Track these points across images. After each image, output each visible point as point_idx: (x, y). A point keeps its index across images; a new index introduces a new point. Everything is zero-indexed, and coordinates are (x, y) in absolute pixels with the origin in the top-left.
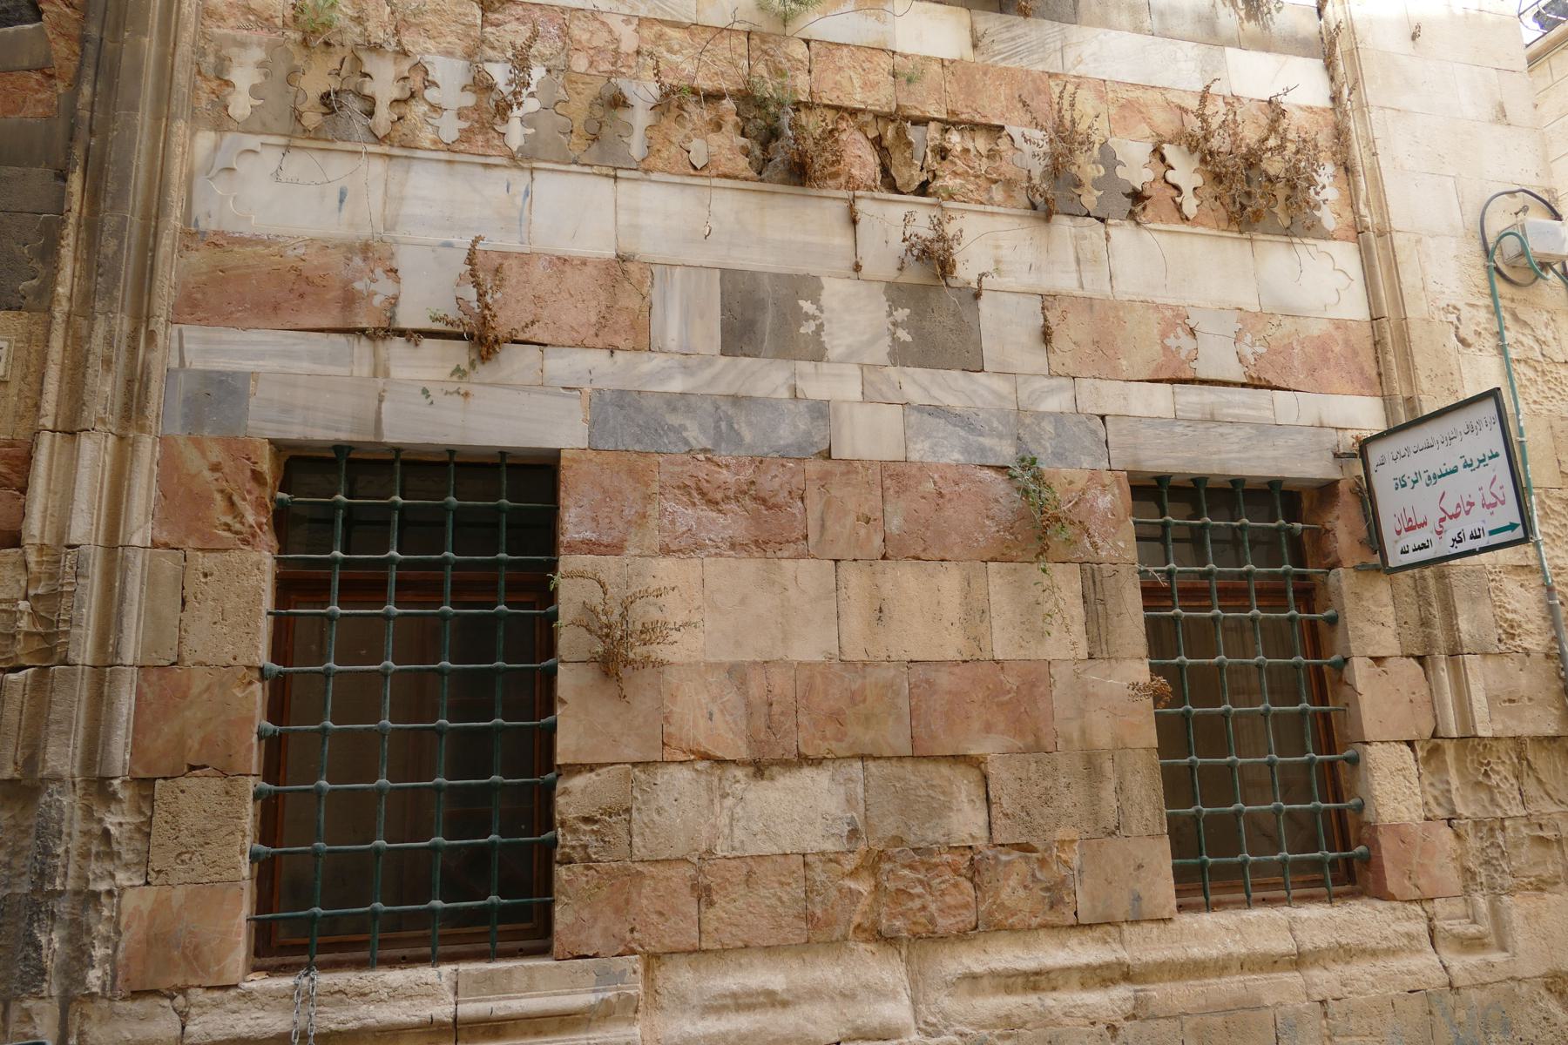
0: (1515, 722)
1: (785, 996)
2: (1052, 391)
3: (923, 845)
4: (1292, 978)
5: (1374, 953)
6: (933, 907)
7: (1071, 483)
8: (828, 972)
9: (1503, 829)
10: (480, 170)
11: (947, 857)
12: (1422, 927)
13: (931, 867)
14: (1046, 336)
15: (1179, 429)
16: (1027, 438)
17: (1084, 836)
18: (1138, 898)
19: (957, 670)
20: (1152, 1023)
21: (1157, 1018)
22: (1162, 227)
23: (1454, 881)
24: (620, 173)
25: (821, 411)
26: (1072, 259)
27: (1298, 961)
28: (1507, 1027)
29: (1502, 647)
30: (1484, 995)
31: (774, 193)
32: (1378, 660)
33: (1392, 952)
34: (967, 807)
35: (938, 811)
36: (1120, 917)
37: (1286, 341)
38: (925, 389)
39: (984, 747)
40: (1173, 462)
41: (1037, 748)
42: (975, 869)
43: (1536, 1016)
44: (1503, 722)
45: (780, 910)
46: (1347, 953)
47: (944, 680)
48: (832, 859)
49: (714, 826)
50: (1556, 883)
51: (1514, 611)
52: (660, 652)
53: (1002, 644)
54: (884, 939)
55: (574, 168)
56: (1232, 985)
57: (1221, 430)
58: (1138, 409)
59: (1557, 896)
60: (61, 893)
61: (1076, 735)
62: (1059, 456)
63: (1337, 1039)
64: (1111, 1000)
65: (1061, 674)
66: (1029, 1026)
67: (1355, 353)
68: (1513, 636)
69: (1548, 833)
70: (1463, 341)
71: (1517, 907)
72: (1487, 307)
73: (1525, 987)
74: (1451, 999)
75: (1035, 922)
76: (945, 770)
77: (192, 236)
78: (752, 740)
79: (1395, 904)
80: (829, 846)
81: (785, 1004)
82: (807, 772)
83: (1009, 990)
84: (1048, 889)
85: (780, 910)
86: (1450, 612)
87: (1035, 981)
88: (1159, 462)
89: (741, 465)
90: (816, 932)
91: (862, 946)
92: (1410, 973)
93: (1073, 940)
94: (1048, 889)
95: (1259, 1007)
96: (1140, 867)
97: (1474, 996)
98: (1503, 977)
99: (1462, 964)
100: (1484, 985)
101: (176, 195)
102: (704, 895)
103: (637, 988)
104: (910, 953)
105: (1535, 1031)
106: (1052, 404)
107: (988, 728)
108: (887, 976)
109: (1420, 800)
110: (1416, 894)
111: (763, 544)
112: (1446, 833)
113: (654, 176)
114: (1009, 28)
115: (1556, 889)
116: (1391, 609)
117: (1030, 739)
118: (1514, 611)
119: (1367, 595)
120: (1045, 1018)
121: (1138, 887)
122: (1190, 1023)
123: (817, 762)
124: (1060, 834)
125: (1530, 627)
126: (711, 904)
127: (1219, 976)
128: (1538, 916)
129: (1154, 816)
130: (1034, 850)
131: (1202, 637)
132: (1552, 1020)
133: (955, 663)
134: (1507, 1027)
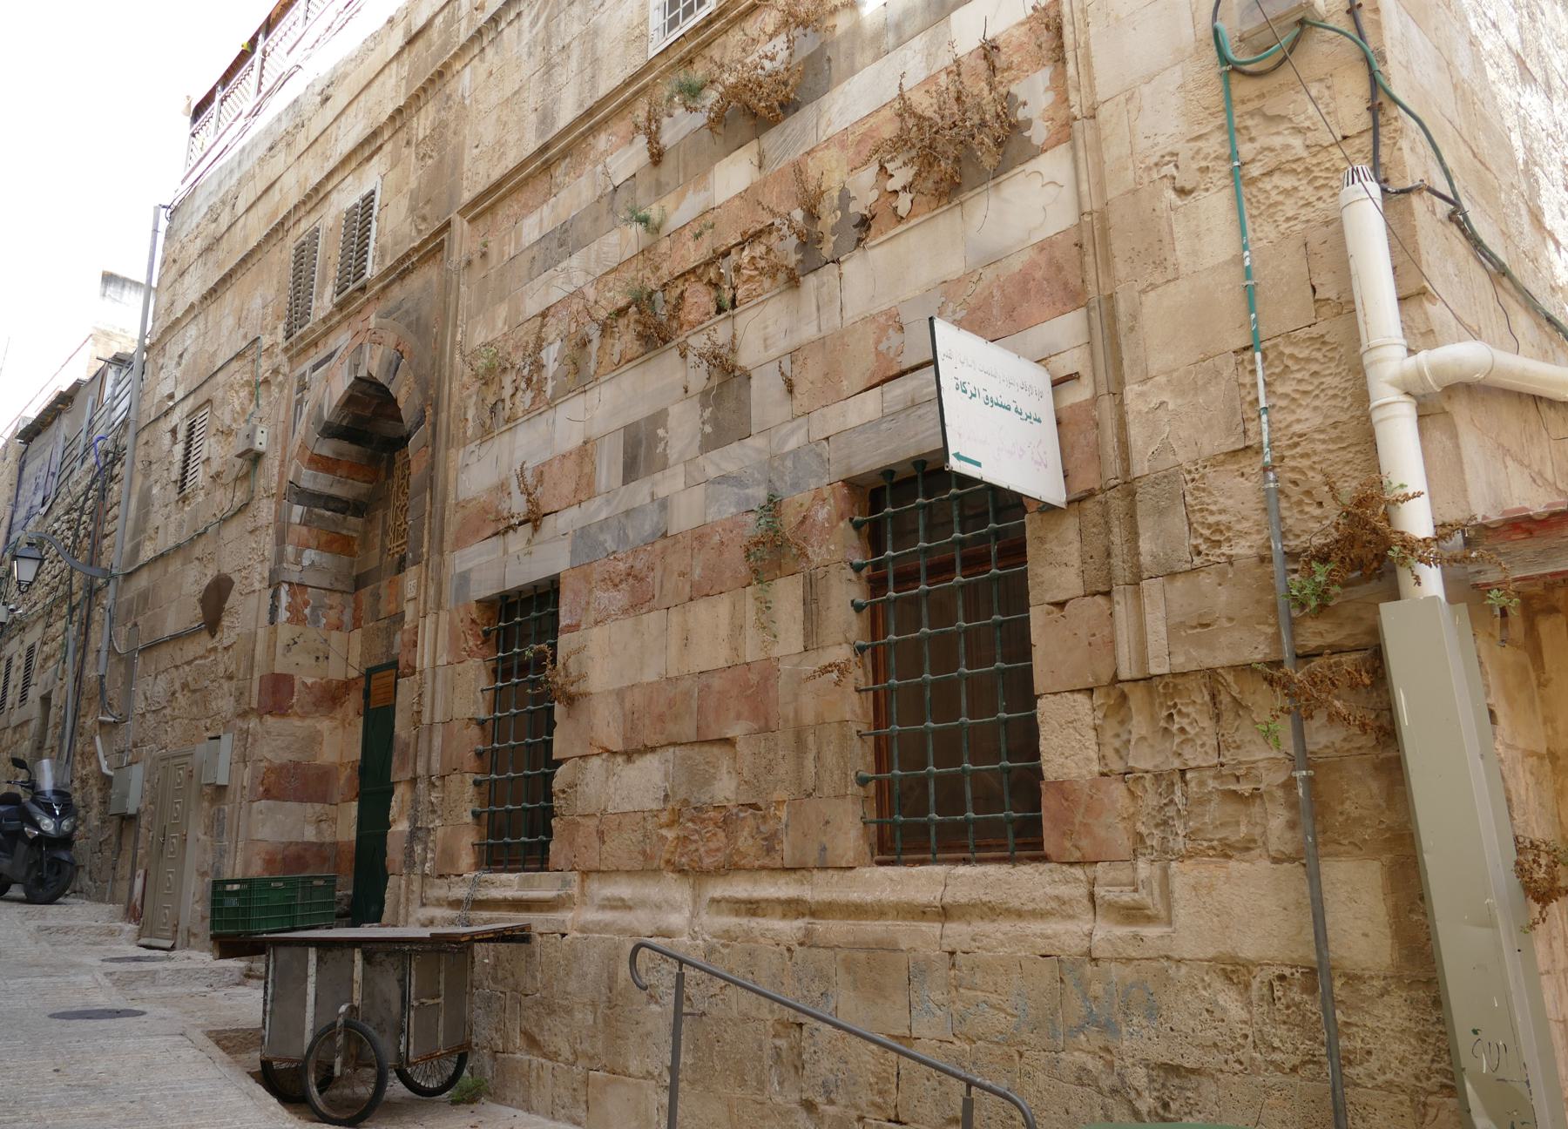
2: (793, 432)
4: (932, 928)
5: (1020, 914)
6: (702, 850)
8: (651, 890)
11: (712, 814)
12: (1082, 891)
14: (790, 387)
16: (774, 478)
18: (824, 849)
20: (814, 950)
23: (1124, 843)
25: (664, 505)
27: (945, 913)
28: (1153, 1012)
29: (1197, 561)
30: (1128, 971)
33: (1041, 915)
34: (725, 777)
35: (708, 780)
36: (810, 864)
37: (987, 293)
38: (718, 465)
39: (736, 730)
41: (766, 729)
42: (727, 822)
46: (992, 911)
47: (717, 683)
48: (655, 814)
50: (1248, 849)
51: (1221, 512)
52: (582, 687)
53: (751, 653)
58: (853, 420)
59: (1245, 865)
61: (791, 715)
62: (795, 486)
64: (789, 928)
65: (785, 667)
67: (1060, 269)
68: (1218, 544)
69: (1245, 788)
73: (1184, 969)
74: (1089, 969)
75: (757, 864)
77: (460, 505)
78: (626, 739)
79: (1052, 865)
80: (655, 806)
81: (630, 908)
82: (649, 757)
83: (737, 913)
84: (765, 839)
86: (1133, 535)
87: (753, 908)
90: (647, 869)
93: (782, 879)
94: (765, 839)
96: (827, 822)
98: (1152, 953)
99: (1107, 933)
100: (1130, 960)
101: (451, 488)
102: (601, 835)
103: (575, 891)
105: (1192, 1023)
107: (738, 717)
108: (678, 896)
110: (1077, 855)
111: (639, 605)
112: (1118, 790)
113: (602, 379)
115: (1247, 856)
116: (1077, 545)
117: (762, 723)
119: (1051, 536)
120: (748, 933)
121: (824, 839)
122: (842, 954)
123: (653, 749)
124: (776, 796)
125: (1245, 525)
131: (909, 613)
132: (1217, 1014)
133: (723, 670)
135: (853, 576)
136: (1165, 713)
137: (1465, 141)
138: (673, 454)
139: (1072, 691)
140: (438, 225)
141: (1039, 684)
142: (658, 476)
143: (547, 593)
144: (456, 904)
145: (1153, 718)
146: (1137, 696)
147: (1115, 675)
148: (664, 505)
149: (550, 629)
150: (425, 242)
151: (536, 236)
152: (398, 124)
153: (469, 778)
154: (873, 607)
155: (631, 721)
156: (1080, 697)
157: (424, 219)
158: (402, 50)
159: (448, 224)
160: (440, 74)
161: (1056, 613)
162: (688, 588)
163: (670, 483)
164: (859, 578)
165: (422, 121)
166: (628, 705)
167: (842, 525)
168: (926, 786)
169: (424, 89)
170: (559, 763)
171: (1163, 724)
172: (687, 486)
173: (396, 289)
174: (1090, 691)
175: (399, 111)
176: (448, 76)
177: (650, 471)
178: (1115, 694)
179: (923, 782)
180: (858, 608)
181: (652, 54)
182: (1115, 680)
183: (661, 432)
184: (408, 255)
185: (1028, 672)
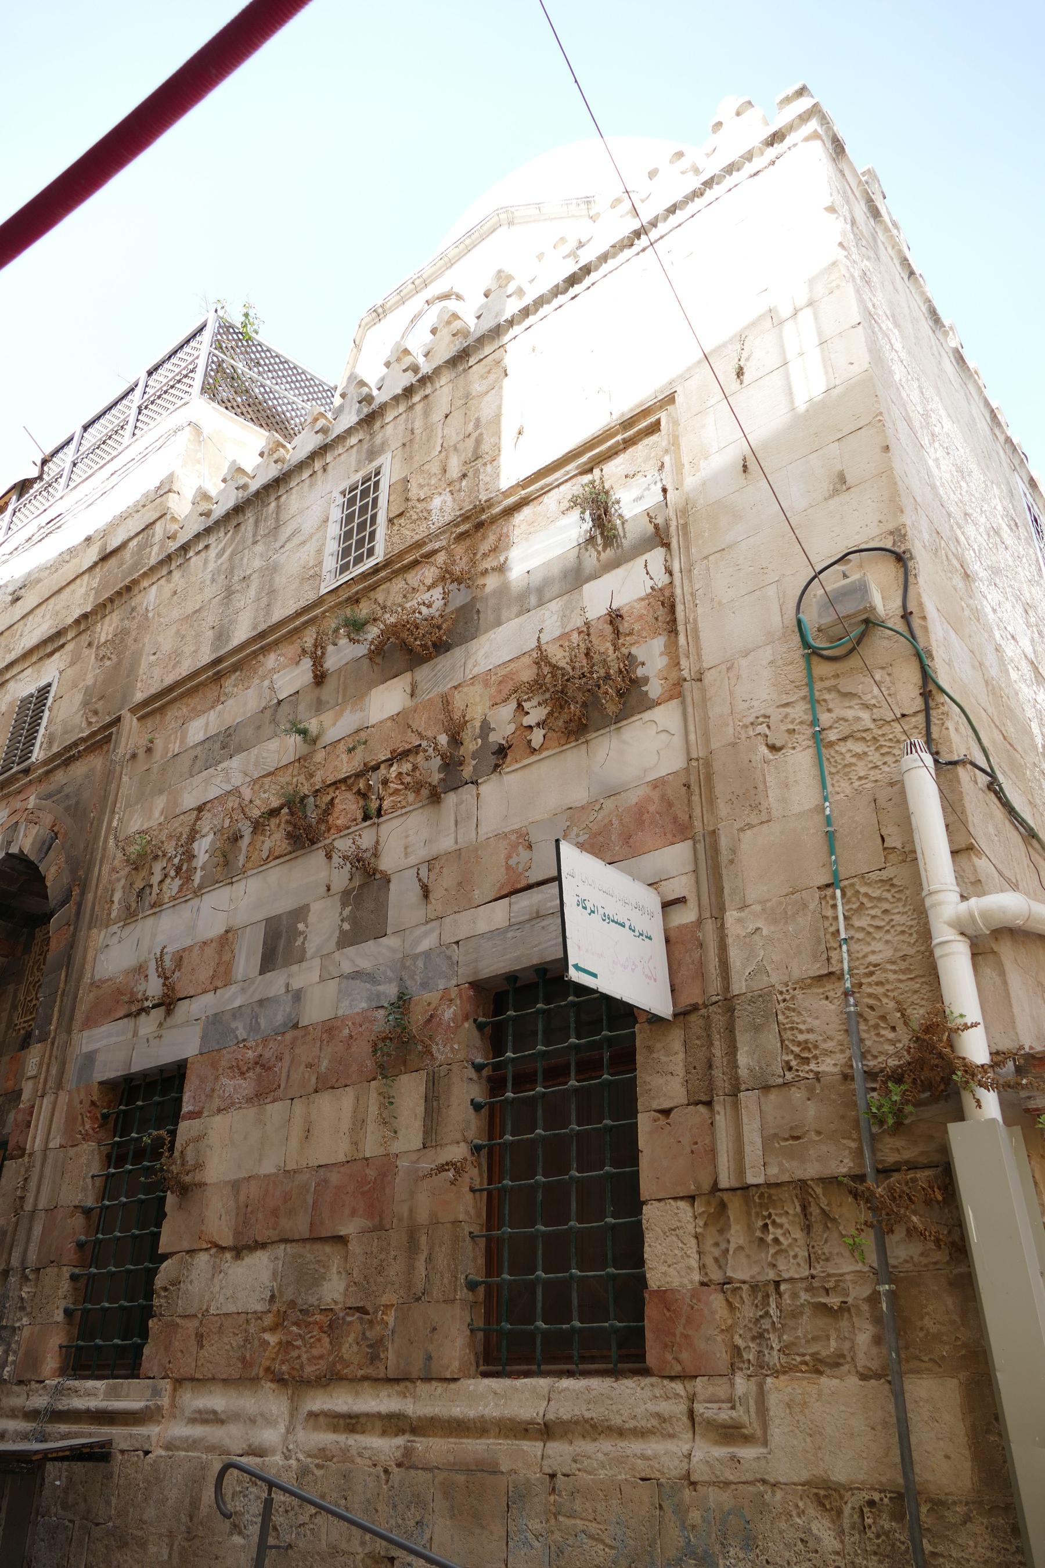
0: (795, 1164)
1: (223, 1417)
2: (426, 934)
3: (305, 1307)
4: (532, 1448)
5: (621, 1433)
6: (305, 1357)
7: (429, 1004)
8: (247, 1402)
9: (779, 1294)
10: (183, 905)
13: (308, 1324)
15: (510, 934)
16: (406, 977)
17: (401, 1301)
18: (429, 1358)
19: (342, 1169)
20: (413, 1472)
21: (417, 1468)
22: (518, 766)
23: (722, 1356)
24: (234, 880)
25: (298, 996)
26: (452, 823)
27: (547, 1431)
28: (749, 1542)
29: (789, 1076)
31: (296, 858)
32: (666, 1112)
33: (641, 1433)
35: (318, 1281)
36: (415, 1375)
37: (606, 821)
38: (353, 961)
40: (502, 964)
41: (380, 1228)
42: (333, 1327)
43: (790, 1535)
44: (781, 1164)
45: (231, 1353)
47: (334, 1178)
48: (259, 1316)
49: (212, 1292)
50: (838, 1365)
51: (810, 1031)
54: (280, 1381)
55: (217, 885)
56: (474, 1447)
57: (543, 923)
58: (483, 927)
60: (6, 1327)
63: (561, 1518)
64: (385, 1446)
65: (403, 1163)
66: (335, 1460)
67: (670, 805)
68: (806, 1061)
69: (834, 1301)
70: (773, 748)
71: (780, 1391)
72: (804, 698)
75: (360, 1373)
76: (328, 1249)
78: (237, 1234)
80: (259, 1308)
81: (222, 1422)
82: (259, 1253)
84: (370, 1346)
85: (231, 1353)
87: (352, 1423)
88: (492, 968)
89: (257, 1045)
91: (269, 1384)
92: (645, 1457)
95: (495, 1472)
96: (434, 1329)
97: (714, 1496)
100: (727, 1484)
103: (165, 1401)
104: (293, 1393)
106: (425, 945)
107: (353, 1213)
108: (274, 1409)
109: (694, 1264)
110: (677, 1369)
111: (261, 1096)
112: (717, 1301)
114: (433, 670)
115: (837, 1372)
118: (810, 1031)
119: (658, 1046)
122: (441, 1476)
123: (263, 1246)
124: (385, 1300)
125: (830, 1045)
126: (202, 1347)
127: (480, 1437)
128: (804, 1404)
129: (450, 1283)
130: (367, 1313)
134: (749, 1542)
136: (760, 1223)
138: (311, 948)
139: (675, 1199)
140: (108, 719)
141: (647, 1187)
142: (295, 968)
146: (735, 1206)
147: (716, 1183)
148: (298, 996)
149: (171, 1115)
150: (94, 734)
151: (200, 737)
153: (66, 1271)
156: (683, 1205)
157: (96, 713)
159: (118, 719)
160: (128, 588)
161: (662, 1121)
162: (313, 1080)
163: (305, 975)
165: (106, 627)
167: (466, 1025)
169: (111, 600)
170: (165, 1257)
171: (758, 1234)
172: (322, 980)
175: (85, 616)
176: (136, 591)
177: (287, 963)
181: (323, 591)
183: (301, 926)
184: (75, 744)
185: (635, 1177)
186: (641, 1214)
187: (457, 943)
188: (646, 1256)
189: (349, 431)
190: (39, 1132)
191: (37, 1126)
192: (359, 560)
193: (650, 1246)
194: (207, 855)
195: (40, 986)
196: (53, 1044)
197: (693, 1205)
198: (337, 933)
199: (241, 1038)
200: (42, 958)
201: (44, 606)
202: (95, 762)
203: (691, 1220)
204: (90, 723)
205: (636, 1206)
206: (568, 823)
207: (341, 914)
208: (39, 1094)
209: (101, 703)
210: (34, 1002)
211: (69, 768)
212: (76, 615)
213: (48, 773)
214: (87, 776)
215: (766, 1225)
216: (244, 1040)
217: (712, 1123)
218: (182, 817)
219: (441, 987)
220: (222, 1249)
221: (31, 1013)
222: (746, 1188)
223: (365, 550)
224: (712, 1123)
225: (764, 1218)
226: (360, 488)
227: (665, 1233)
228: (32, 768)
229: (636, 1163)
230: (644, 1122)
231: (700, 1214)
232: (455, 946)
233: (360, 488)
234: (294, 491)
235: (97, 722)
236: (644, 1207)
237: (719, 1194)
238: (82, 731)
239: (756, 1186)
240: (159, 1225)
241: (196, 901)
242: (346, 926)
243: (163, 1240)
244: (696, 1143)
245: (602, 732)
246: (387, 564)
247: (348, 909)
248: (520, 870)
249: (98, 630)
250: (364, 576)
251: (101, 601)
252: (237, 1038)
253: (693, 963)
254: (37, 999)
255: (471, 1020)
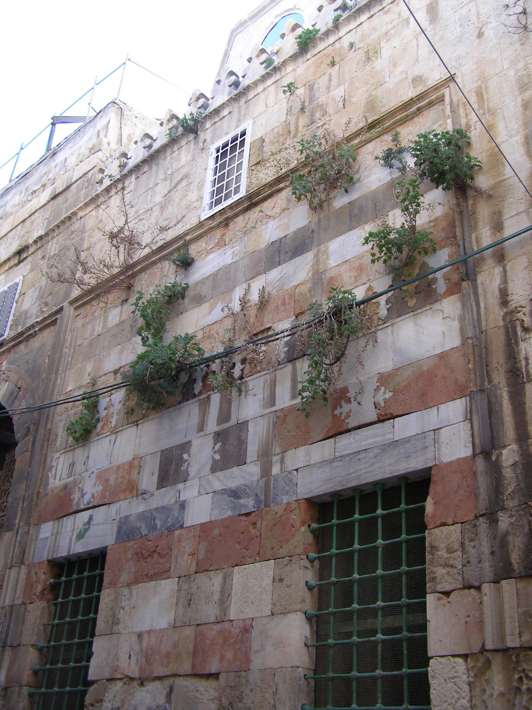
7: (276, 513)
38: (222, 482)
78: (141, 669)
135: (308, 564)
136: (516, 676)
137: (472, 256)
138: (193, 471)
139: (453, 656)
140: (55, 309)
141: (433, 649)
142: (180, 486)
143: (98, 557)
144: (288, 336)
145: (509, 679)
146: (497, 661)
147: (483, 646)
148: (183, 506)
149: (96, 584)
150: (45, 319)
151: (116, 321)
152: (39, 245)
153: (25, 690)
154: (320, 587)
155: (148, 657)
156: (459, 660)
157: (46, 304)
158: (49, 202)
159: (62, 309)
160: (69, 218)
161: (445, 600)
162: (194, 564)
163: (189, 491)
164: (312, 566)
165: (54, 245)
166: (145, 645)
167: (303, 529)
168: (352, 587)
169: (58, 226)
170: (92, 683)
171: (515, 684)
172: (200, 494)
173: (22, 346)
174: (465, 657)
175: (41, 238)
176: (74, 219)
177: (176, 482)
178: (482, 660)
179: (351, 554)
180: (310, 588)
181: (203, 218)
182: (483, 650)
183: (185, 456)
184: (33, 326)
185: (424, 640)
186: (427, 665)
187: (297, 470)
188: (431, 696)
189: (223, 106)
190: (9, 592)
191: (7, 588)
192: (227, 197)
193: (435, 689)
194: (121, 405)
195: (9, 493)
196: (17, 532)
197: (466, 661)
198: (211, 462)
199: (143, 534)
200: (10, 474)
201: (15, 230)
202: (47, 337)
203: (465, 671)
204: (43, 312)
205: (425, 661)
206: (378, 384)
207: (214, 448)
208: (8, 567)
209: (50, 297)
210: (5, 504)
211: (29, 343)
212: (35, 238)
213: (14, 346)
214: (40, 348)
215: (521, 678)
216: (146, 535)
217: (481, 602)
218: (103, 377)
219: (285, 501)
220: (132, 679)
221: (3, 511)
222: (506, 650)
223: (221, 152)
224: (481, 602)
225: (519, 672)
226: (230, 145)
227: (445, 681)
228: (5, 343)
229: (425, 631)
230: (430, 599)
231: (472, 667)
232: (295, 472)
233: (230, 145)
234: (183, 148)
235: (48, 311)
236: (431, 661)
237: (485, 653)
238: (37, 317)
239: (513, 648)
240: (88, 660)
241: (113, 437)
242: (217, 457)
243: (91, 671)
244: (469, 616)
245: (403, 317)
246: (249, 197)
247: (219, 445)
248: (343, 417)
249: (49, 247)
250: (231, 207)
251: (51, 227)
252: (141, 533)
253: (468, 486)
254: (7, 502)
255: (306, 526)
